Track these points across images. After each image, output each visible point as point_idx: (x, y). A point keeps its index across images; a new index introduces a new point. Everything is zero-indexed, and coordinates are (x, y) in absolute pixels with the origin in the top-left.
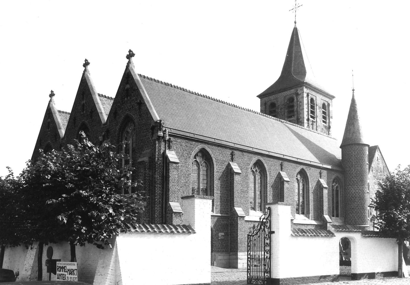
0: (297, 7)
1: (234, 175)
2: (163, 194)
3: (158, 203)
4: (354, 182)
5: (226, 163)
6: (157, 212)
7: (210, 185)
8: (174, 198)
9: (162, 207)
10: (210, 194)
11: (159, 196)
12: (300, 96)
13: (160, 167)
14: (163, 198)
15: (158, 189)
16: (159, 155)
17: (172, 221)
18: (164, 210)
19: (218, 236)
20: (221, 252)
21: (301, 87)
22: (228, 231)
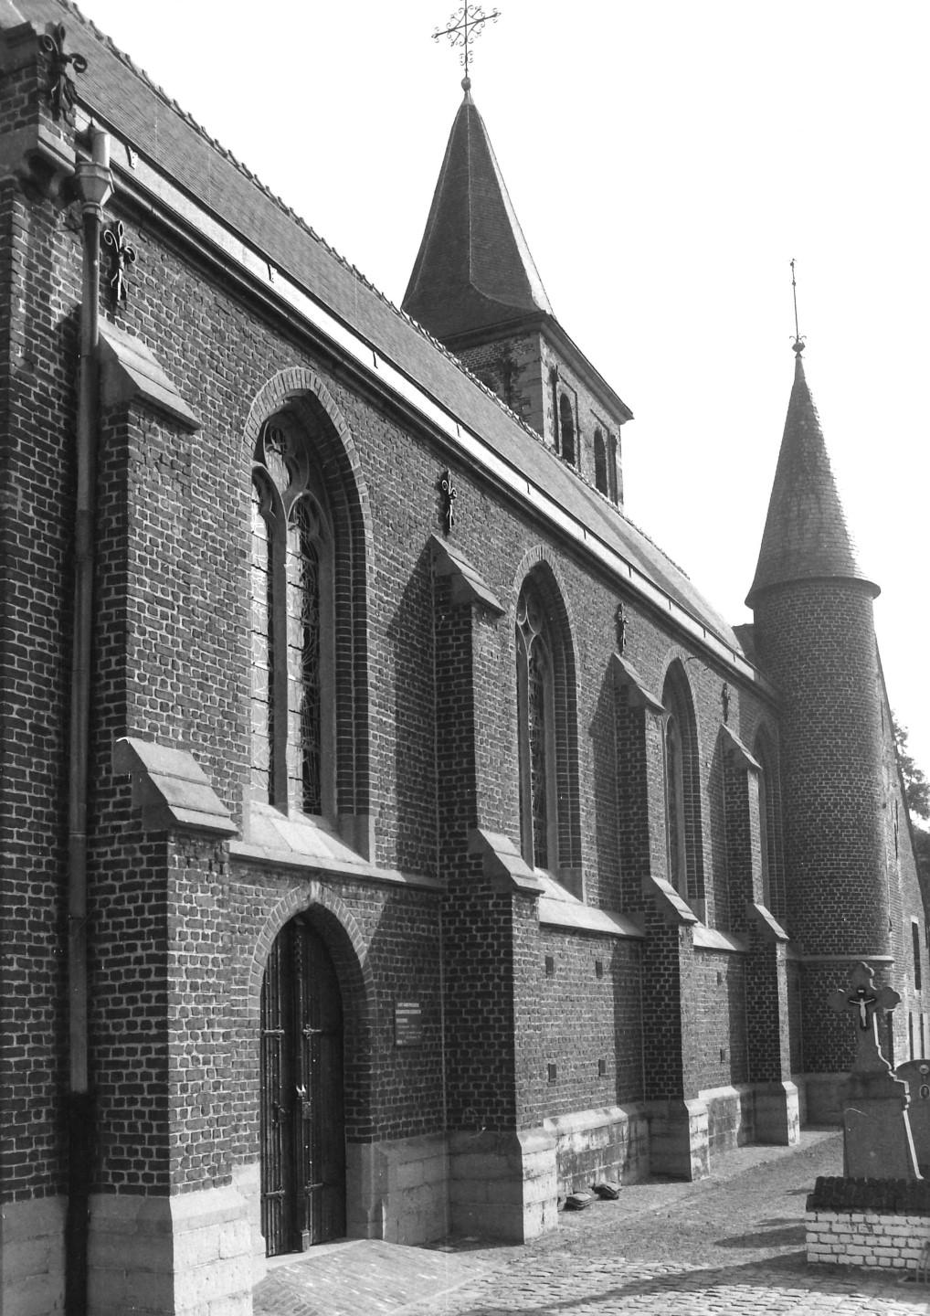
0: (465, 26)
1: (474, 621)
2: (65, 666)
3: (28, 739)
4: (832, 754)
5: (420, 539)
6: (21, 824)
7: (339, 665)
8: (164, 707)
9: (63, 785)
10: (339, 725)
11: (33, 678)
12: (523, 377)
13: (44, 435)
14: (66, 699)
15: (28, 617)
16: (38, 326)
17: (164, 909)
18: (77, 809)
19: (393, 1022)
20: (407, 1134)
21: (527, 334)
22: (436, 988)
